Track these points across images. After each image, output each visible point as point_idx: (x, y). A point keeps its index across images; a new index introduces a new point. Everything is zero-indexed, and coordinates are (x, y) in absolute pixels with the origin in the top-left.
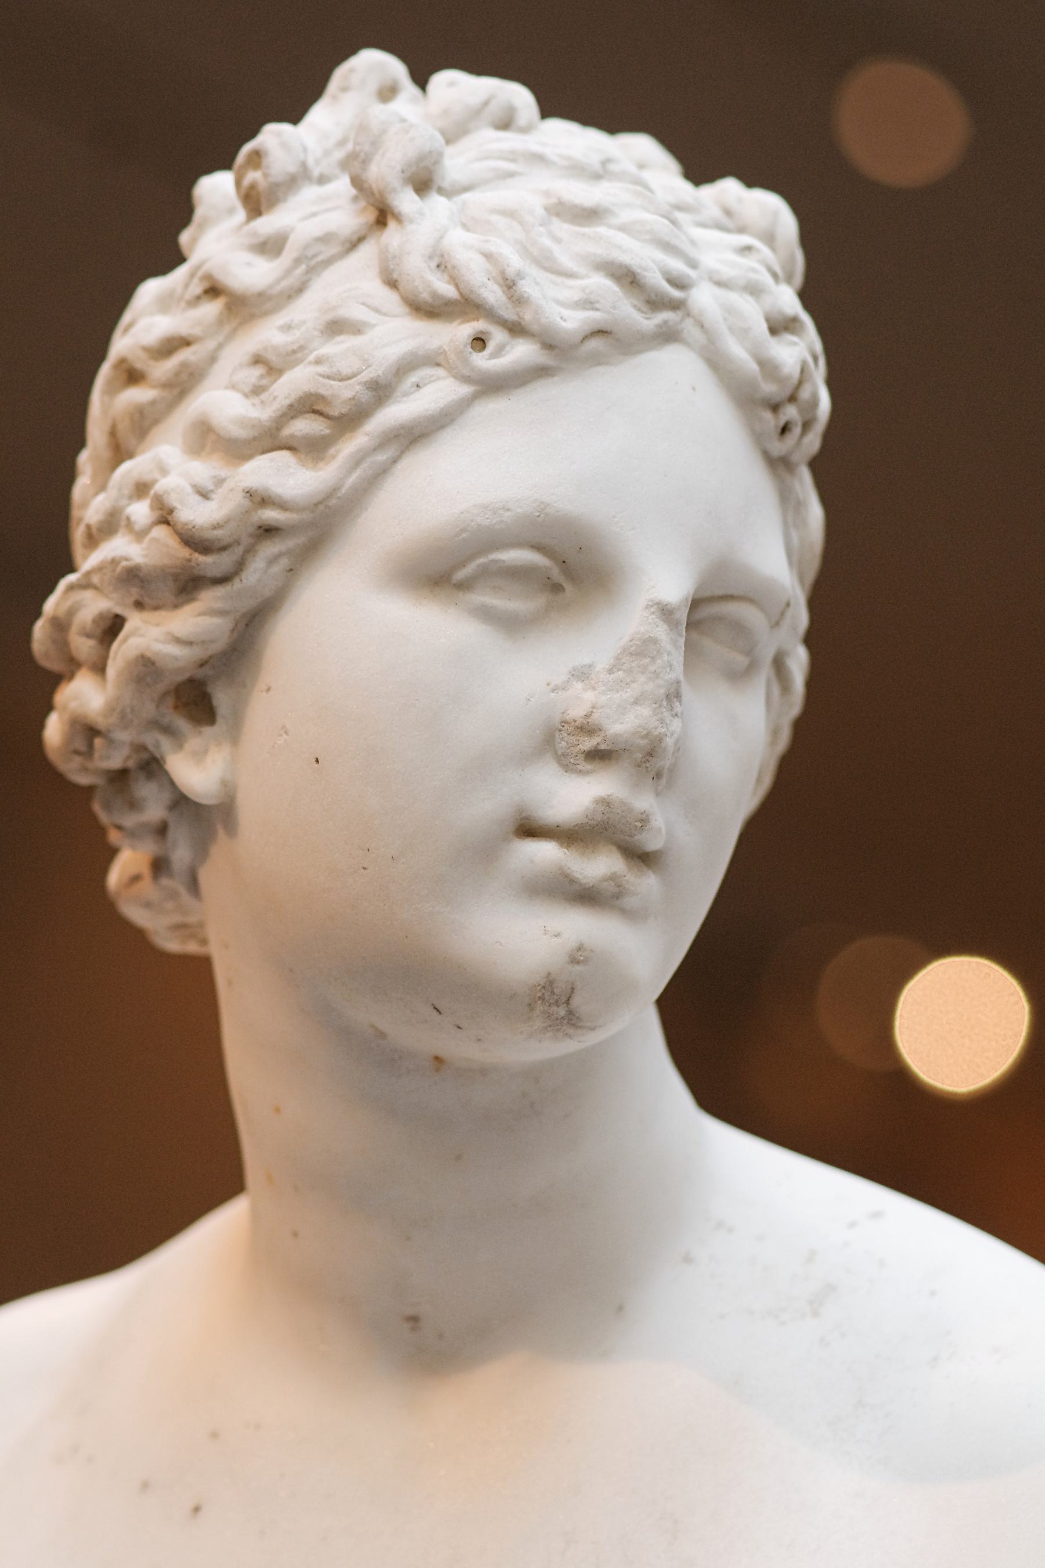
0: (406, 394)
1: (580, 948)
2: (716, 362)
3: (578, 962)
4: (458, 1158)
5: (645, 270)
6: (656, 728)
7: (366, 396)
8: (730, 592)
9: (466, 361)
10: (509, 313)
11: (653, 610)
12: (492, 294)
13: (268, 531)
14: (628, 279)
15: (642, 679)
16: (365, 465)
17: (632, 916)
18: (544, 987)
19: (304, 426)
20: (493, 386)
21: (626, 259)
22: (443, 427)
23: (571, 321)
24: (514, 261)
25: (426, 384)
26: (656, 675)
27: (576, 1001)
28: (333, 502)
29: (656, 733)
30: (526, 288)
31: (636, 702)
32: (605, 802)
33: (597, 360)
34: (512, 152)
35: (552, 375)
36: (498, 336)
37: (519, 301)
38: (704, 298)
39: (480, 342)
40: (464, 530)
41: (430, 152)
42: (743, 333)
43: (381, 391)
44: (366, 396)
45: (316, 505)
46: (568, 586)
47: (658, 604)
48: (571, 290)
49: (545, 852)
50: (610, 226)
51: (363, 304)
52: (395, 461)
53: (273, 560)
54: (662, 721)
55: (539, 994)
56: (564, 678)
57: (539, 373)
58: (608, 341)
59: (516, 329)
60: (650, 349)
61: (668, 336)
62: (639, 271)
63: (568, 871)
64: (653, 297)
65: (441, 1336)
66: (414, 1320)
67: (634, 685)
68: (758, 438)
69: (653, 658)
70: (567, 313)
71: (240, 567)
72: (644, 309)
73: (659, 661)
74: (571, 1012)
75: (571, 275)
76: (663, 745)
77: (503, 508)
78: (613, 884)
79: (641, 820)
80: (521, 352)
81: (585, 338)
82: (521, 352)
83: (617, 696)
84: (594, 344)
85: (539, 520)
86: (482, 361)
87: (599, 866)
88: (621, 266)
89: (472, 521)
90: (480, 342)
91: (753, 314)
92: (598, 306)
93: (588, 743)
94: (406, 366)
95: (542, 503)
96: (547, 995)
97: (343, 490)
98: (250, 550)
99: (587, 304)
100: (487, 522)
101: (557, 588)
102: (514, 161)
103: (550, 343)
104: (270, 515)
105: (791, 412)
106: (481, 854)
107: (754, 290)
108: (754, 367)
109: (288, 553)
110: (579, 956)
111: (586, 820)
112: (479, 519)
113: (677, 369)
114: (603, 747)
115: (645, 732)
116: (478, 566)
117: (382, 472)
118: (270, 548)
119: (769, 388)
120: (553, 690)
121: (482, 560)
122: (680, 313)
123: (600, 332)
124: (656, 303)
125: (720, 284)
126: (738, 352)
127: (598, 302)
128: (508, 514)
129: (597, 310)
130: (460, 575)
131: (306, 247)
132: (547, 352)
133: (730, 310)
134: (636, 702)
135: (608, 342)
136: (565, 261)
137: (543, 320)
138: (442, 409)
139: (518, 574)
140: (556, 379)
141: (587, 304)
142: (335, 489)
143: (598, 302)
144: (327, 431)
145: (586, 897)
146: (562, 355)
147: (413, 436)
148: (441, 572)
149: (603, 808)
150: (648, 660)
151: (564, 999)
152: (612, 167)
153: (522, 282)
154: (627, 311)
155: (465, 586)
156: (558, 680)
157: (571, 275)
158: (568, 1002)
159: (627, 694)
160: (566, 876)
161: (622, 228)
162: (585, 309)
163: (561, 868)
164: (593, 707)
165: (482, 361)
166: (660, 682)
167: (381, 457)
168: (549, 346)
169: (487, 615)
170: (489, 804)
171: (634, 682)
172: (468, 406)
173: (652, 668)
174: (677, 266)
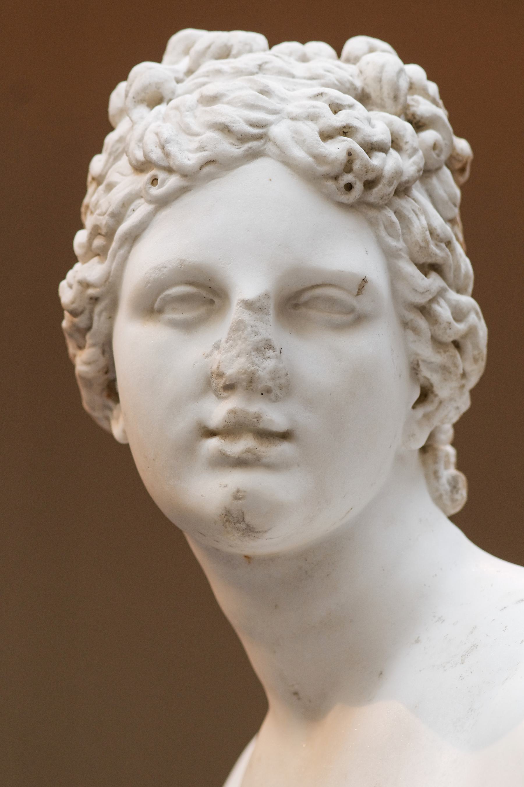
0: (129, 216)
1: (238, 491)
2: (287, 162)
3: (239, 499)
4: (276, 606)
5: (234, 123)
6: (249, 368)
7: (111, 222)
8: (314, 283)
9: (147, 193)
10: (164, 163)
11: (240, 305)
12: (156, 155)
13: (95, 300)
14: (225, 129)
15: (240, 342)
16: (117, 257)
17: (270, 467)
18: (226, 515)
19: (98, 242)
20: (163, 203)
22: (144, 230)
23: (188, 156)
25: (137, 209)
26: (246, 339)
27: (247, 519)
28: (111, 279)
29: (249, 370)
30: (171, 148)
31: (238, 356)
32: (233, 412)
33: (211, 177)
34: (208, 72)
35: (190, 190)
36: (162, 176)
37: (167, 155)
38: (280, 130)
39: (154, 181)
40: (148, 282)
41: (150, 84)
42: (301, 143)
44: (111, 222)
45: (106, 281)
46: (216, 300)
47: (243, 301)
48: (195, 143)
49: (213, 444)
50: (223, 103)
51: (118, 172)
52: (129, 252)
53: (100, 315)
54: (253, 363)
55: (225, 519)
56: (210, 349)
57: (181, 192)
58: (214, 167)
59: (170, 170)
60: (242, 165)
61: (253, 155)
62: (229, 124)
63: (224, 452)
64: (240, 137)
65: (310, 701)
66: (296, 693)
67: (237, 347)
68: (328, 197)
69: (242, 330)
70: (191, 155)
71: (91, 319)
72: (236, 144)
73: (246, 332)
74: (248, 525)
75: (197, 135)
76: (256, 376)
77: (163, 267)
78: (249, 454)
79: (256, 418)
80: (172, 182)
81: (201, 167)
82: (172, 182)
83: (229, 354)
84: (207, 169)
85: (182, 269)
86: (155, 191)
87: (238, 447)
88: (220, 124)
89: (150, 277)
90: (154, 181)
91: (310, 131)
92: (206, 148)
93: (222, 382)
95: (181, 260)
96: (231, 519)
97: (112, 273)
98: (92, 312)
100: (156, 276)
101: (212, 302)
102: (208, 76)
104: (91, 292)
105: (348, 178)
106: (187, 450)
107: (313, 118)
108: (310, 160)
109: (105, 309)
110: (238, 496)
111: (226, 423)
112: (153, 275)
113: (263, 169)
114: (227, 383)
115: (243, 371)
116: (161, 299)
117: (125, 259)
118: (98, 308)
119: (323, 169)
120: (206, 357)
121: (161, 296)
122: (263, 141)
123: (210, 162)
124: (243, 138)
125: (293, 119)
126: (299, 154)
127: (206, 146)
128: (166, 269)
129: (206, 150)
130: (156, 306)
131: (113, 146)
132: (184, 178)
133: (296, 132)
134: (238, 356)
135: (214, 167)
136: (195, 127)
137: (177, 163)
138: (140, 221)
139: (183, 299)
140: (192, 191)
141: (202, 148)
142: (109, 273)
143: (206, 146)
144: (105, 243)
145: (241, 463)
147: (133, 237)
148: (151, 307)
149: (233, 415)
150: (241, 332)
151: (241, 520)
152: (267, 66)
153: (167, 145)
154: (228, 147)
155: (160, 311)
156: (208, 350)
157: (197, 135)
158: (243, 520)
159: (235, 352)
160: (224, 454)
161: (228, 103)
162: (201, 151)
163: (220, 451)
164: (219, 363)
165: (155, 191)
166: (248, 342)
167: (122, 252)
168: (185, 175)
169: (175, 324)
170: (182, 424)
171: (236, 345)
172: (154, 216)
173: (243, 336)
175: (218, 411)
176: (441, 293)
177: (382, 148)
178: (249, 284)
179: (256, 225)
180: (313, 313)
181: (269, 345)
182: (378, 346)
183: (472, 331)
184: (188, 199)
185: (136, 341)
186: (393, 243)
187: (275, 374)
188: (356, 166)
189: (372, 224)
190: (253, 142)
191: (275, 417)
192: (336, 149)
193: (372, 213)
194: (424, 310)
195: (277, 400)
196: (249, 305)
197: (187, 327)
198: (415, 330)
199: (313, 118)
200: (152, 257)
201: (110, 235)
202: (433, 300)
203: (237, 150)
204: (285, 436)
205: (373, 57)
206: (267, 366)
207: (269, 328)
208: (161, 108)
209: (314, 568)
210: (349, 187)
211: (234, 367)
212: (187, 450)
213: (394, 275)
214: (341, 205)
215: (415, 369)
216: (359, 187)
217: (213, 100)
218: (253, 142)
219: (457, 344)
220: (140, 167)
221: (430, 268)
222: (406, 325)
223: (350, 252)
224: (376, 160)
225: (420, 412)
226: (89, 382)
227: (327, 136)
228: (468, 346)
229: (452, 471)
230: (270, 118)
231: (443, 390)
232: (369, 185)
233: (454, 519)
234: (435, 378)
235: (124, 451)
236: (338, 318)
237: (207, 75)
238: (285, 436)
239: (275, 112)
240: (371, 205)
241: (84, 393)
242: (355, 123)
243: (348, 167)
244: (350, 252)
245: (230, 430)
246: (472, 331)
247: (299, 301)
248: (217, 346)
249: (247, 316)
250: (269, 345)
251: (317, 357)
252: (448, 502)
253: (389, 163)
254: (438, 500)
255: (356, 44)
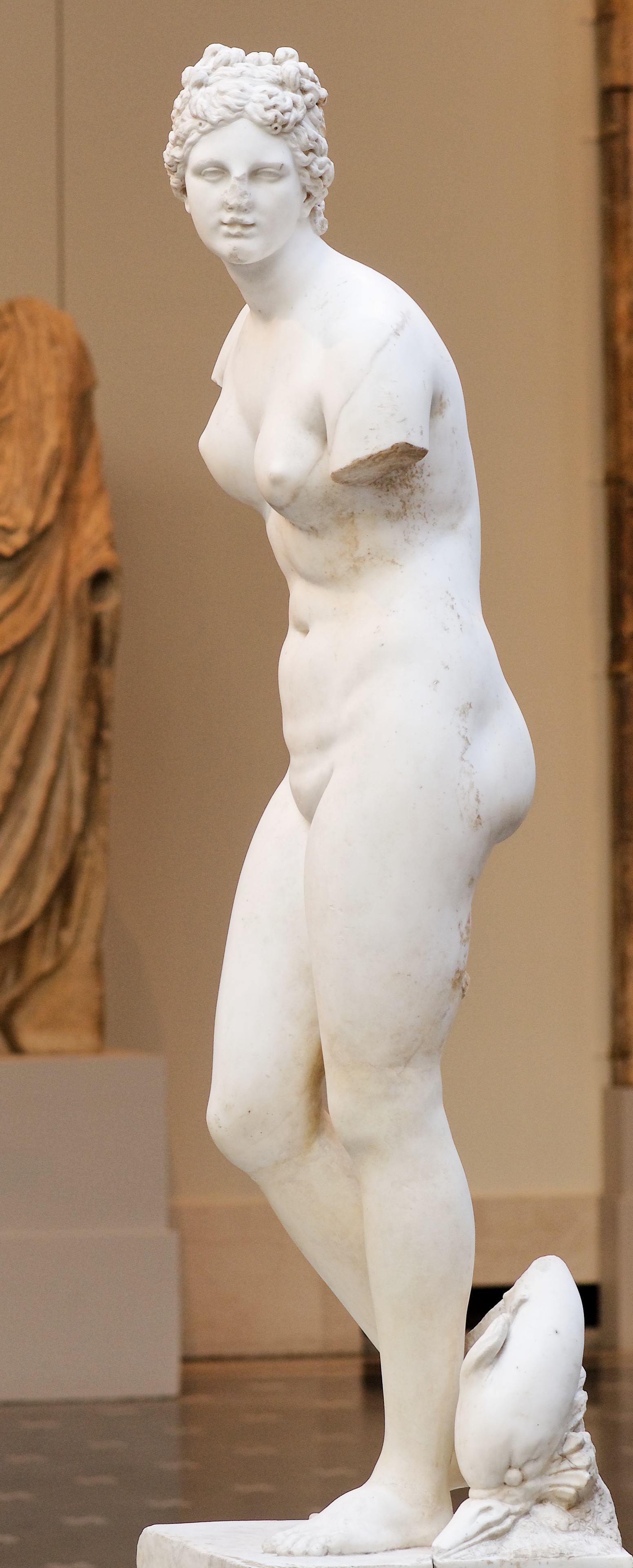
2: (252, 120)
12: (201, 115)
14: (228, 107)
20: (204, 133)
21: (227, 103)
23: (215, 119)
24: (205, 107)
30: (207, 113)
33: (223, 126)
36: (203, 123)
38: (249, 108)
43: (187, 136)
49: (225, 229)
57: (212, 130)
58: (224, 122)
68: (269, 133)
80: (207, 126)
86: (201, 129)
87: (235, 230)
90: (200, 124)
91: (261, 107)
94: (190, 131)
99: (219, 115)
103: (212, 124)
105: (276, 125)
106: (215, 229)
107: (261, 102)
117: (190, 152)
119: (266, 123)
124: (235, 111)
126: (257, 118)
135: (224, 122)
136: (217, 105)
141: (219, 115)
145: (236, 236)
146: (216, 126)
147: (193, 144)
148: (199, 172)
155: (204, 175)
170: (213, 220)
174: (241, 102)
175: (227, 217)
176: (314, 160)
177: (289, 111)
178: (238, 169)
179: (241, 145)
180: (264, 177)
181: (246, 193)
182: (289, 187)
183: (327, 172)
184: (214, 133)
185: (193, 183)
186: (294, 146)
187: (248, 204)
188: (279, 120)
189: (286, 139)
190: (239, 112)
191: (248, 219)
192: (270, 115)
193: (286, 136)
194: (307, 168)
195: (249, 212)
196: (238, 179)
197: (214, 182)
198: (304, 176)
199: (261, 102)
200: (200, 155)
201: (184, 141)
202: (312, 163)
203: (232, 116)
204: (253, 225)
205: (289, 62)
206: (244, 202)
207: (244, 187)
208: (203, 89)
209: (262, 270)
210: (276, 128)
211: (232, 202)
212: (215, 229)
213: (294, 157)
214: (273, 135)
215: (304, 188)
216: (280, 128)
217: (222, 93)
218: (239, 112)
219: (321, 177)
220: (196, 117)
221: (309, 151)
222: (300, 174)
223: (276, 153)
224: (286, 117)
225: (307, 203)
226: (176, 189)
227: (267, 109)
228: (326, 177)
229: (322, 217)
230: (245, 102)
231: (315, 194)
232: (284, 126)
233: (322, 237)
234: (312, 191)
235: (188, 217)
236: (273, 178)
237: (221, 75)
238: (253, 225)
239: (247, 99)
240: (285, 133)
241: (174, 191)
242: (278, 103)
243: (275, 121)
244: (276, 153)
245: (232, 224)
246: (327, 172)
247: (255, 173)
248: (226, 192)
249: (237, 183)
250: (246, 193)
251: (266, 194)
252: (319, 231)
253: (291, 117)
254: (316, 231)
255: (281, 52)
